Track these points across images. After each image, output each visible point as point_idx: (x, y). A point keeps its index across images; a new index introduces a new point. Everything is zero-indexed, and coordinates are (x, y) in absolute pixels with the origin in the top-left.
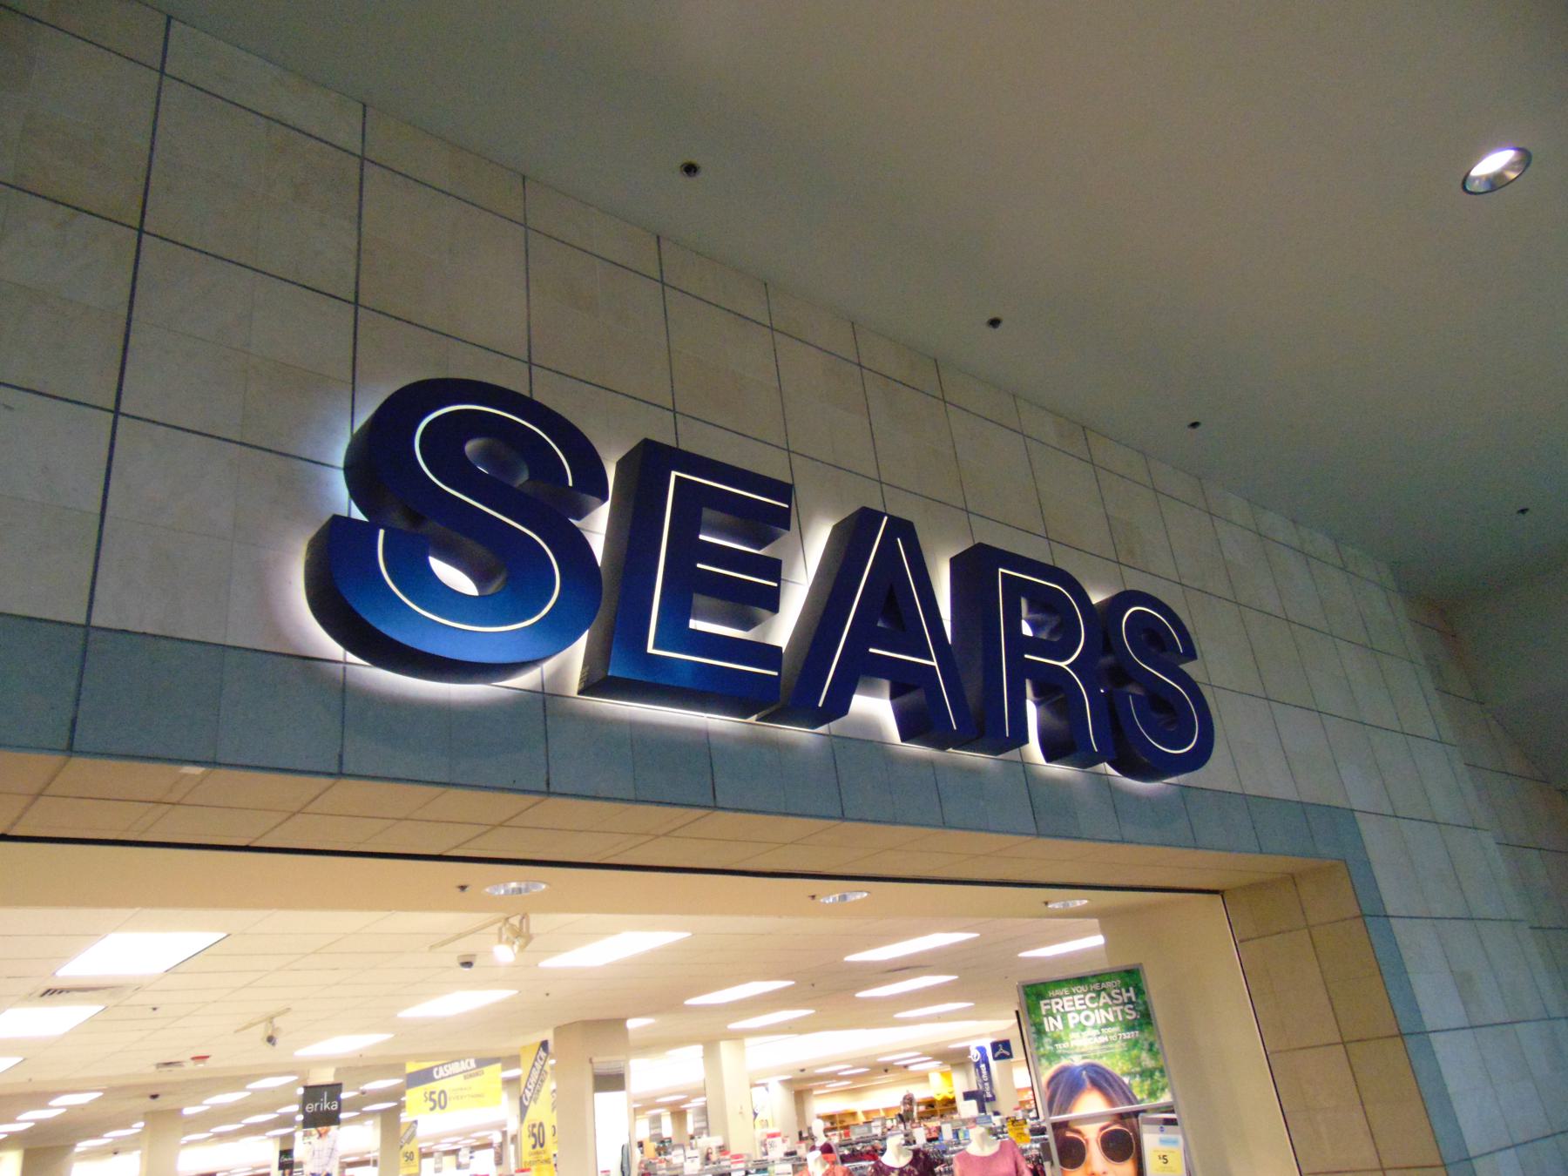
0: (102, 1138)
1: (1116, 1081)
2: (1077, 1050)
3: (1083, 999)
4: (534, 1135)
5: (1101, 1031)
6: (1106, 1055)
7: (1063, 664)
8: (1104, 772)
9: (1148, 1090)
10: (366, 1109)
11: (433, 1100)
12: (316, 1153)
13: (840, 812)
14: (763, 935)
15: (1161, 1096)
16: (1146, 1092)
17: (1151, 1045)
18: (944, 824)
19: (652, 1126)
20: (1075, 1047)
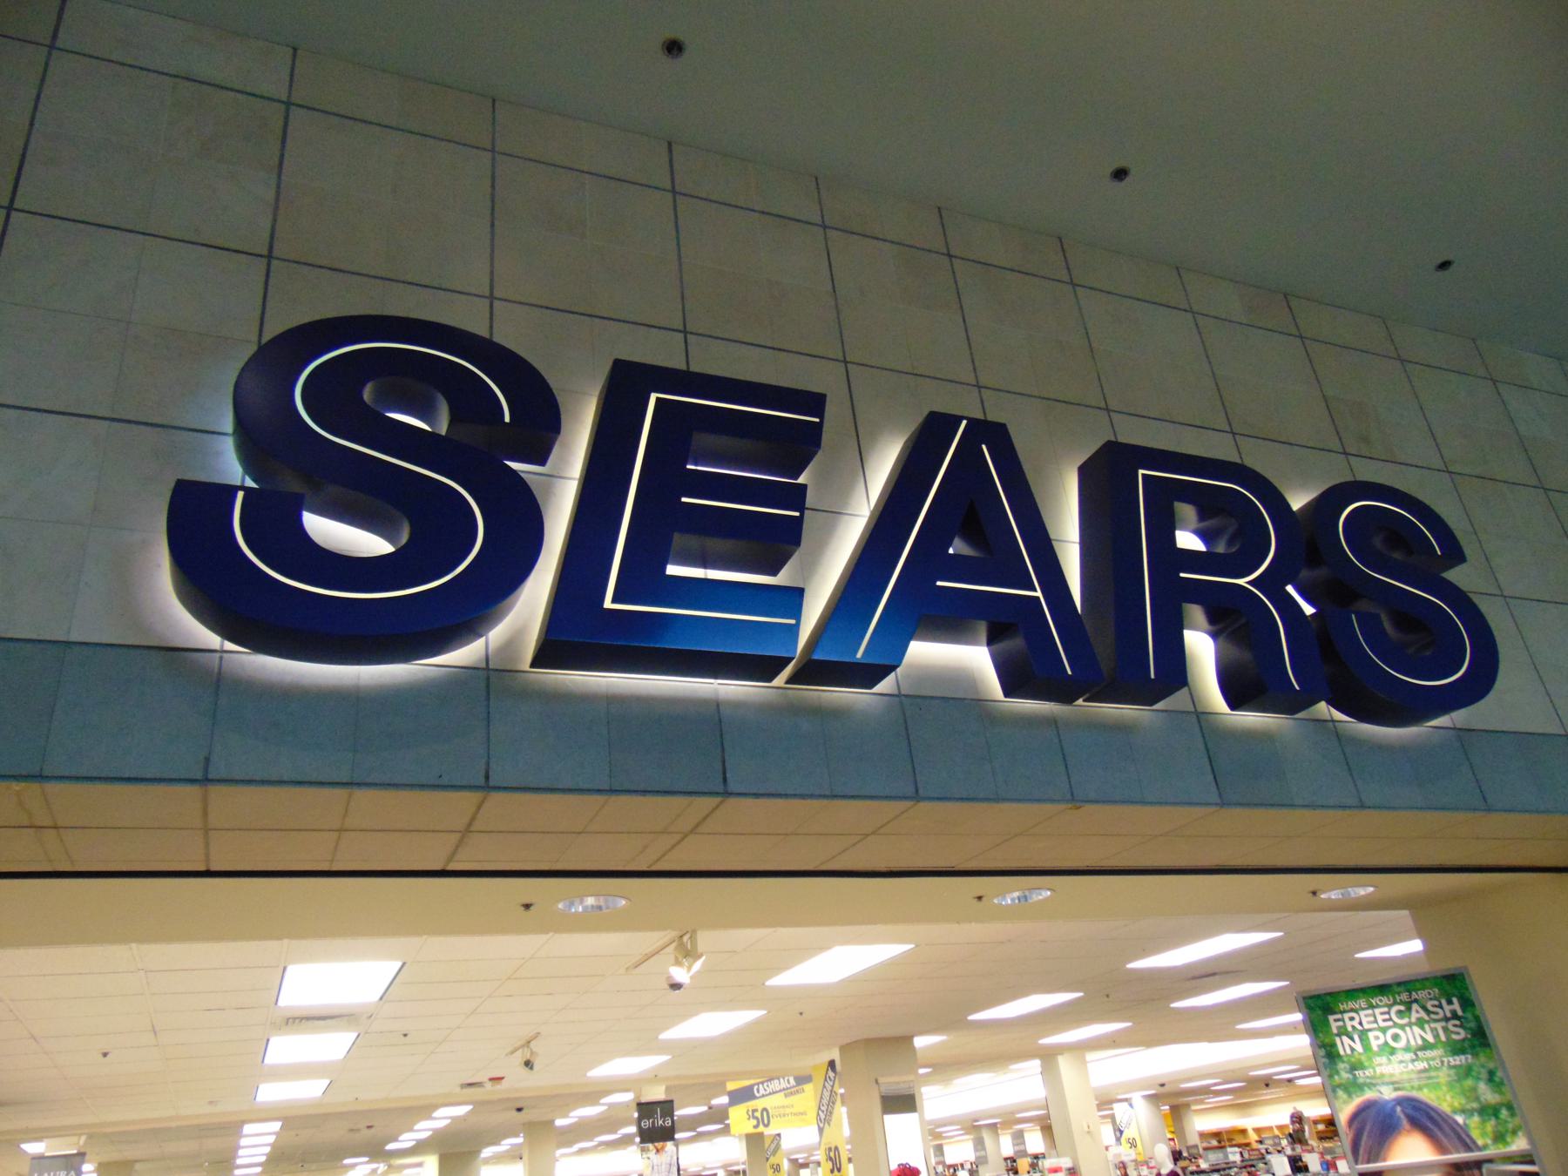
0: (499, 1145)
1: (1443, 1119)
2: (1387, 1079)
3: (1389, 1013)
4: (831, 1159)
5: (1416, 1055)
6: (1427, 1086)
7: (1241, 582)
8: (1329, 718)
9: (1494, 1132)
10: (700, 1129)
11: (757, 1118)
12: (655, 1167)
13: (914, 790)
14: (1003, 943)
15: (1513, 1142)
16: (1491, 1135)
17: (1491, 1074)
18: (1074, 799)
19: (1015, 1142)
20: (1382, 1075)
